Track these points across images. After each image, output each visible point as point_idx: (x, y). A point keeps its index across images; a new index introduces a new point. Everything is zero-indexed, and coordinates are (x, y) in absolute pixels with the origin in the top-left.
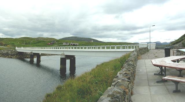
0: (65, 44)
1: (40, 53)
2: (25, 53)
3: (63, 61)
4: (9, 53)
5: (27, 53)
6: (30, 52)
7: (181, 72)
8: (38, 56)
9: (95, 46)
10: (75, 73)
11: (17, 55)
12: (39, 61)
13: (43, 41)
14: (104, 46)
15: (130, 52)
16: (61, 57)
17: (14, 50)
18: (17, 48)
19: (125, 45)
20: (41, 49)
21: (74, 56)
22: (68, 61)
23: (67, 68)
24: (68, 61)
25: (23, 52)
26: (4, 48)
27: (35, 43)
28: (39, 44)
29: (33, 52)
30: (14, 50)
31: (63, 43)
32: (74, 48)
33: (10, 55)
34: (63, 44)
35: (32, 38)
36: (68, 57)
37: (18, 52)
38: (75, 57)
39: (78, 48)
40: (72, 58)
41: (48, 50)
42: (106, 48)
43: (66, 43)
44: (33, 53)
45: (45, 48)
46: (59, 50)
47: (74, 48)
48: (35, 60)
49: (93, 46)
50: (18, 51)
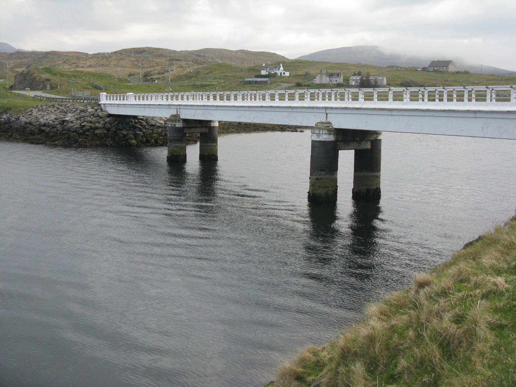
0: (326, 80)
2: (146, 120)
5: (153, 118)
6: (166, 114)
7: (382, 386)
10: (335, 210)
15: (292, 88)
16: (315, 138)
17: (90, 110)
18: (104, 99)
21: (376, 133)
23: (382, 186)
25: (135, 117)
26: (41, 99)
29: (183, 116)
30: (90, 110)
32: (361, 96)
34: (317, 81)
37: (110, 115)
38: (380, 137)
39: (383, 97)
41: (244, 104)
43: (331, 75)
44: (185, 121)
46: (297, 103)
47: (361, 96)
49: (451, 89)
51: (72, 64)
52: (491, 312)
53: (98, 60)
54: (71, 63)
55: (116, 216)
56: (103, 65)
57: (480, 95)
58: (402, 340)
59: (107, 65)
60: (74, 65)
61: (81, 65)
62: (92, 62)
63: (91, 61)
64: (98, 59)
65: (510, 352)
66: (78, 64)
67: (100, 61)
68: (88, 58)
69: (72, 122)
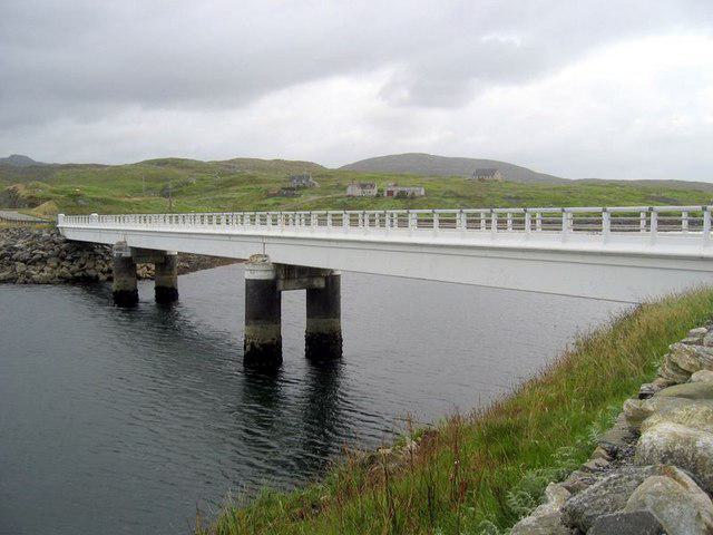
1: (172, 247)
3: (263, 300)
4: (16, 249)
8: (163, 261)
9: (488, 210)
11: (63, 259)
12: (167, 296)
13: (252, 180)
14: (600, 209)
17: (45, 234)
19: (373, 212)
20: (304, 232)
22: (294, 304)
24: (294, 304)
27: (208, 190)
28: (233, 193)
31: (345, 189)
33: (25, 262)
35: (201, 163)
36: (290, 274)
40: (323, 292)
42: (567, 223)
43: (363, 186)
45: (223, 220)
48: (147, 292)
50: (71, 236)
57: (474, 221)
69: (22, 250)
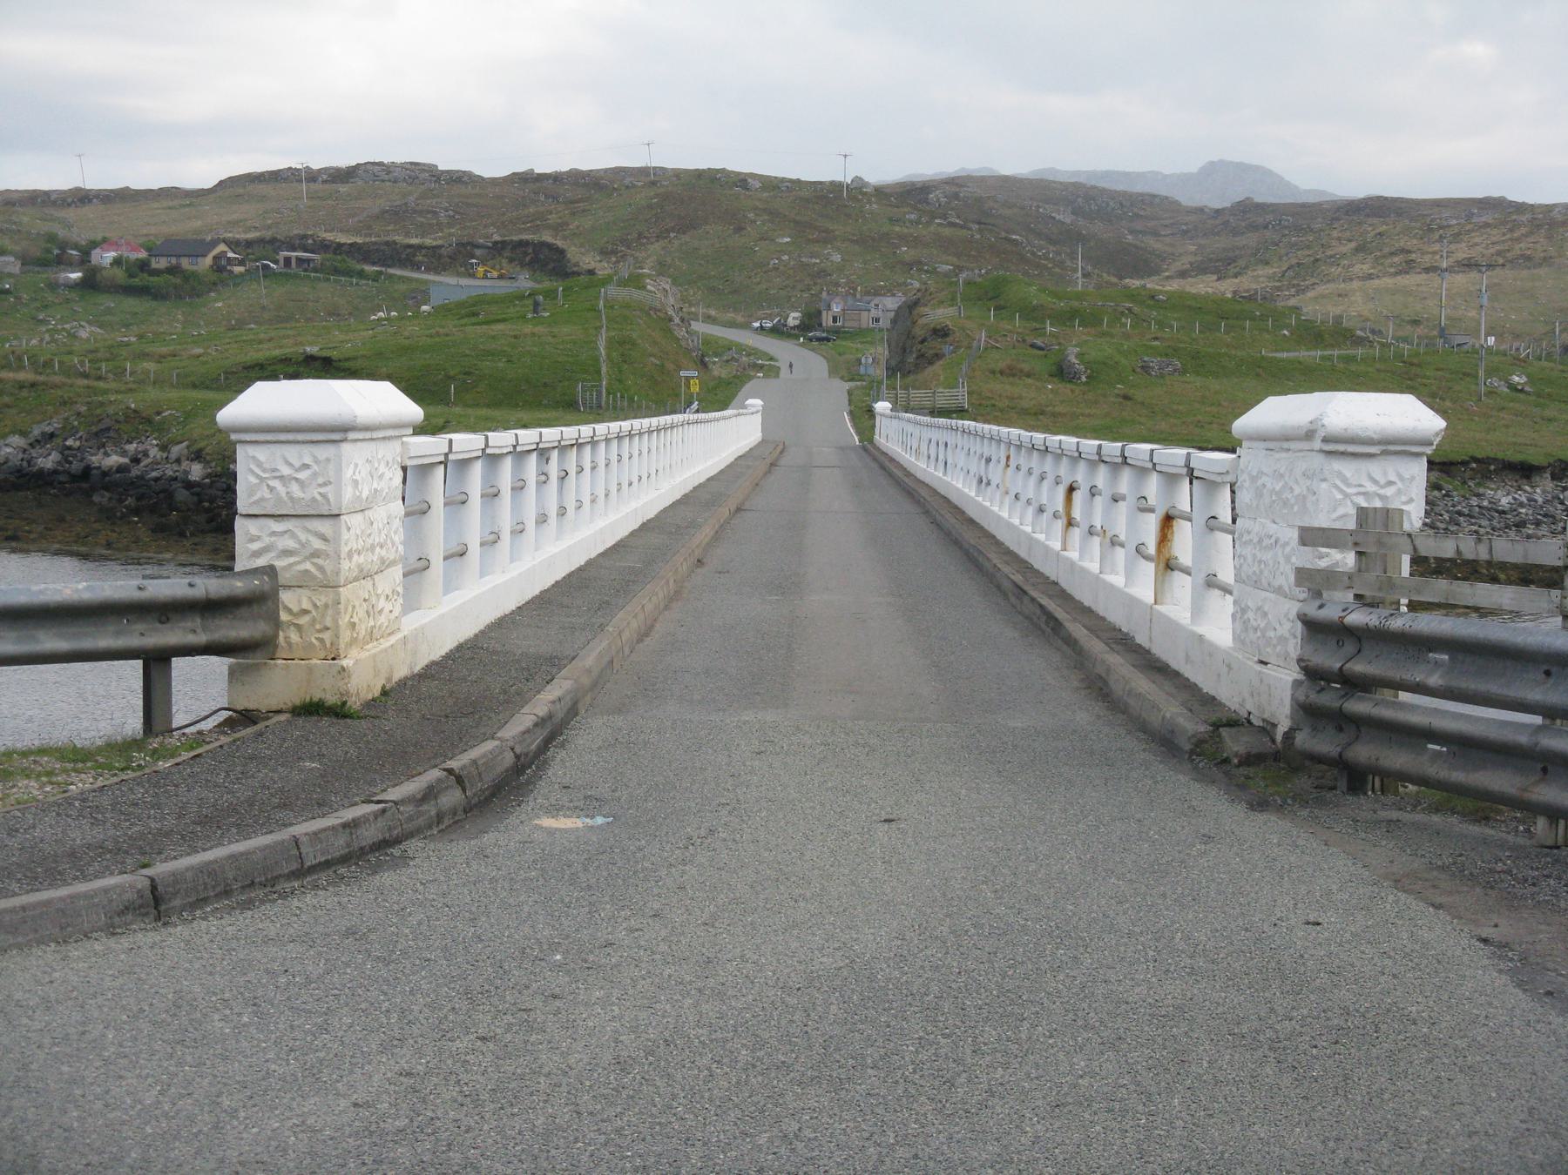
51: (1392, 254)
52: (1047, 406)
53: (1508, 236)
54: (1386, 250)
55: (468, 785)
56: (1529, 258)
58: (208, 450)
59: (1546, 260)
60: (1396, 259)
61: (1427, 258)
62: (1479, 246)
63: (1477, 240)
64: (1511, 230)
65: (128, 546)
66: (1413, 256)
67: (1518, 240)
68: (1469, 227)
